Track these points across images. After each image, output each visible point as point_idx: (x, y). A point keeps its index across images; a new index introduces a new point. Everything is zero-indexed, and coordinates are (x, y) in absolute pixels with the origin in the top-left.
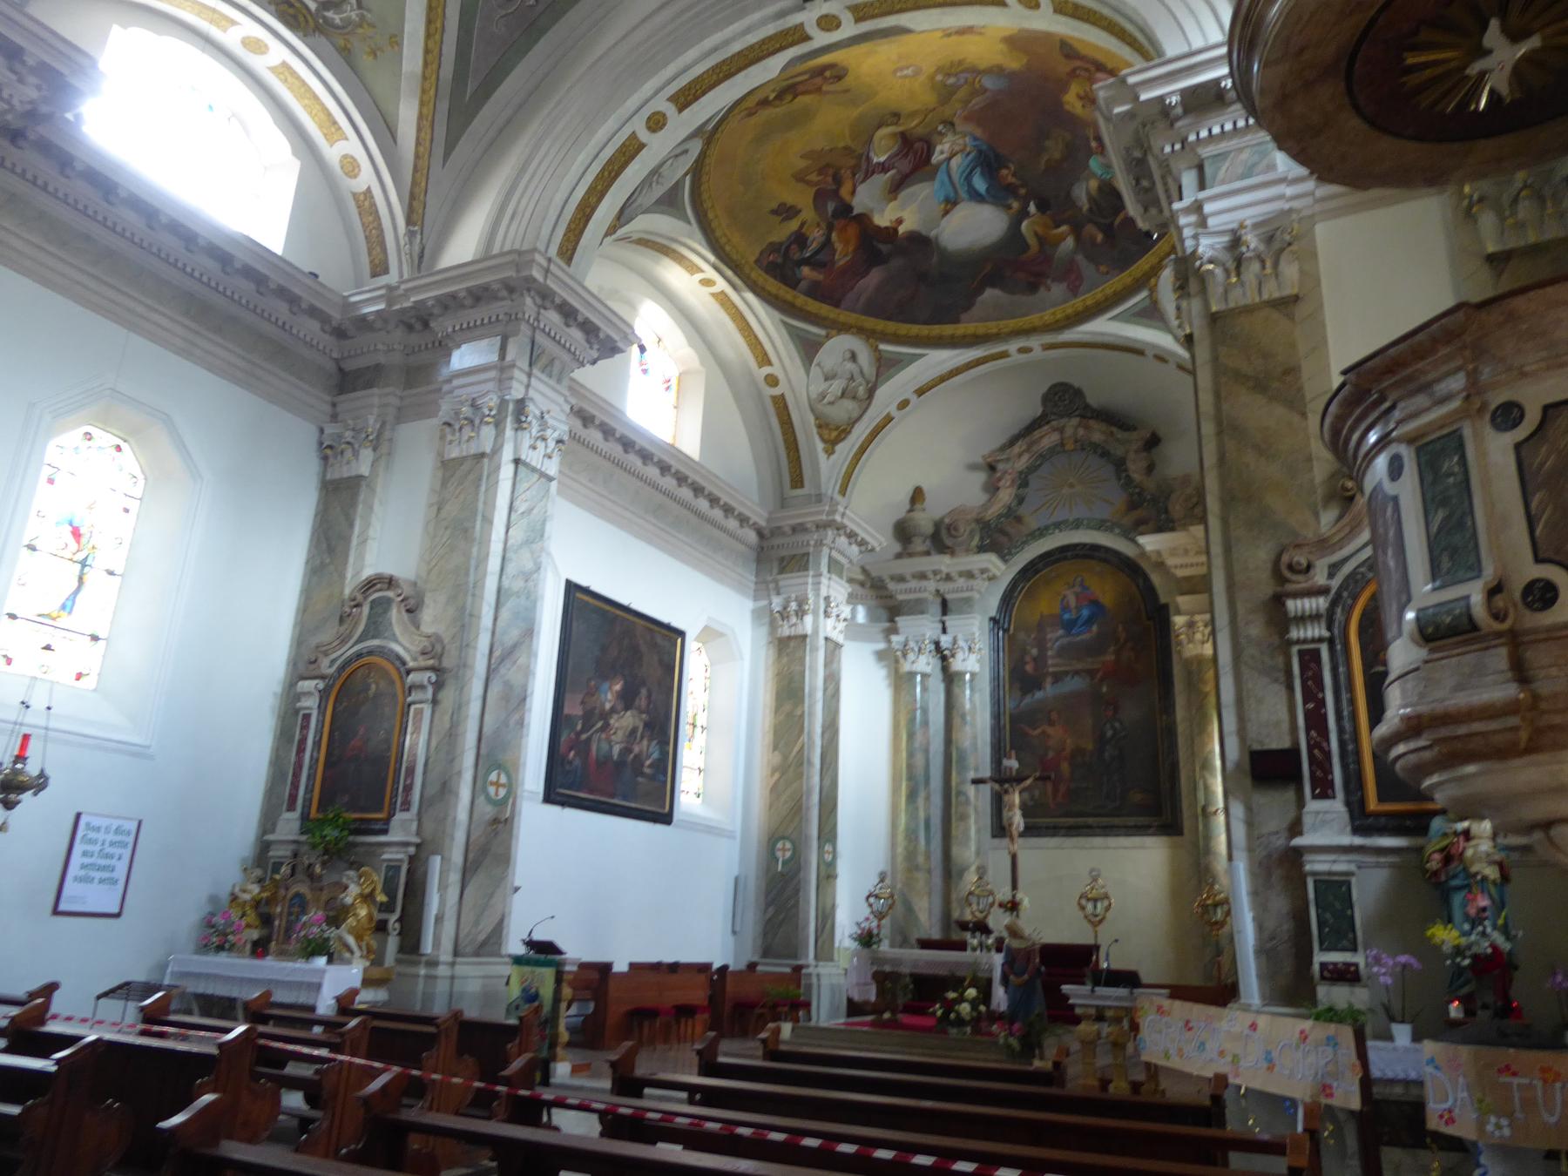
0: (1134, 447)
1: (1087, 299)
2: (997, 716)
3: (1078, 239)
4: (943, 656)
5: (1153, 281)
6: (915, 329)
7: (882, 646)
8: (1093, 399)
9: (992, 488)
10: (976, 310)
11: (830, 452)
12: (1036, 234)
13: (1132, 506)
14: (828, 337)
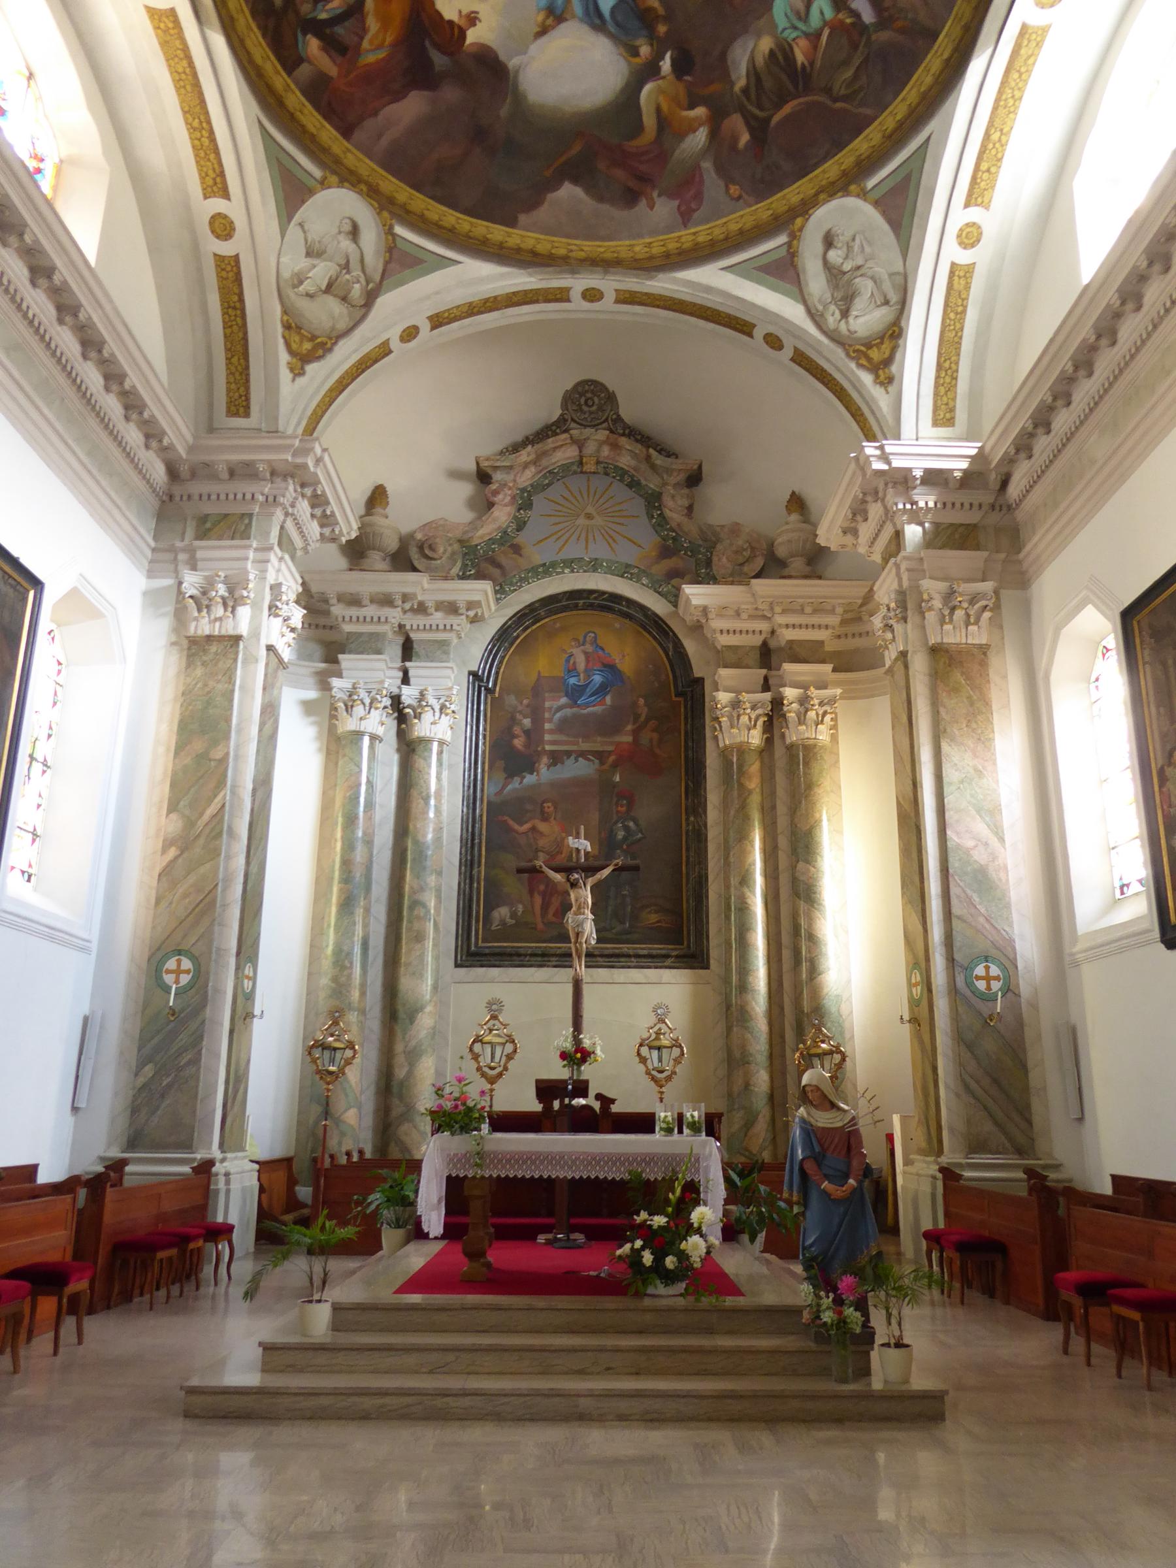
0: (673, 480)
1: (700, 232)
2: (471, 802)
3: (714, 134)
4: (400, 713)
5: (799, 221)
6: (452, 218)
7: (312, 694)
8: (628, 411)
9: (484, 505)
10: (542, 213)
11: (297, 372)
12: (658, 110)
13: (666, 552)
14: (323, 184)
